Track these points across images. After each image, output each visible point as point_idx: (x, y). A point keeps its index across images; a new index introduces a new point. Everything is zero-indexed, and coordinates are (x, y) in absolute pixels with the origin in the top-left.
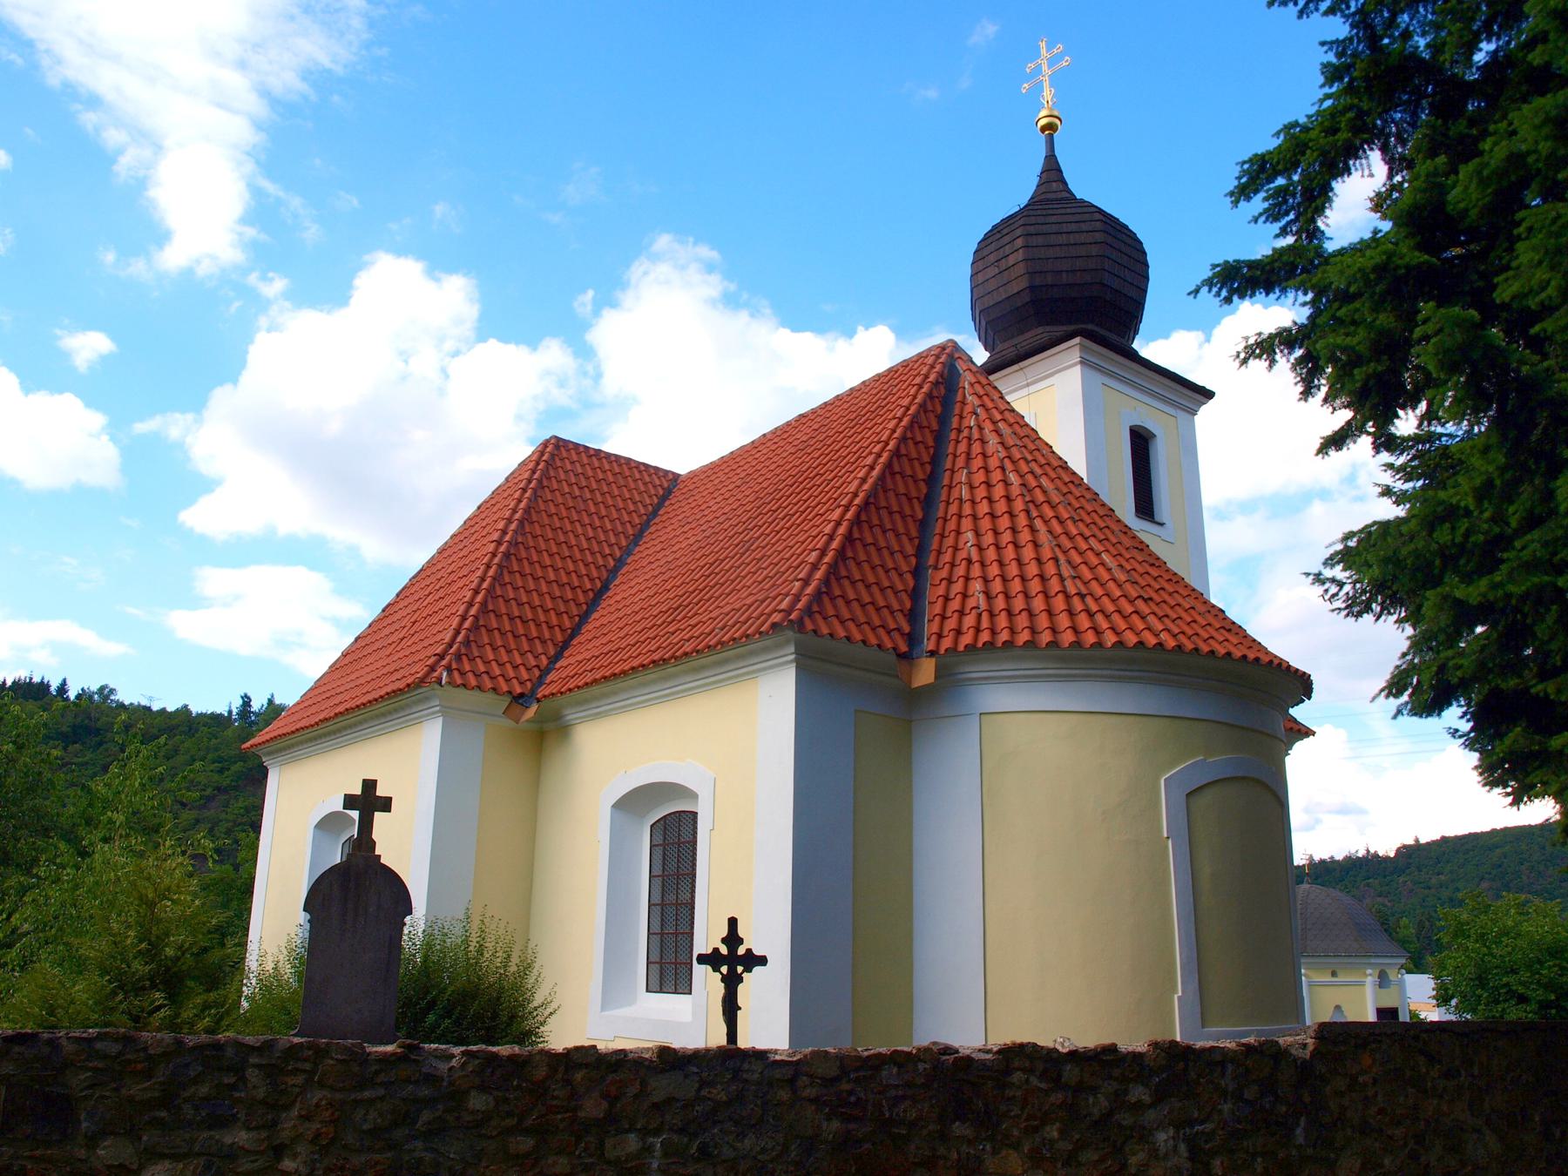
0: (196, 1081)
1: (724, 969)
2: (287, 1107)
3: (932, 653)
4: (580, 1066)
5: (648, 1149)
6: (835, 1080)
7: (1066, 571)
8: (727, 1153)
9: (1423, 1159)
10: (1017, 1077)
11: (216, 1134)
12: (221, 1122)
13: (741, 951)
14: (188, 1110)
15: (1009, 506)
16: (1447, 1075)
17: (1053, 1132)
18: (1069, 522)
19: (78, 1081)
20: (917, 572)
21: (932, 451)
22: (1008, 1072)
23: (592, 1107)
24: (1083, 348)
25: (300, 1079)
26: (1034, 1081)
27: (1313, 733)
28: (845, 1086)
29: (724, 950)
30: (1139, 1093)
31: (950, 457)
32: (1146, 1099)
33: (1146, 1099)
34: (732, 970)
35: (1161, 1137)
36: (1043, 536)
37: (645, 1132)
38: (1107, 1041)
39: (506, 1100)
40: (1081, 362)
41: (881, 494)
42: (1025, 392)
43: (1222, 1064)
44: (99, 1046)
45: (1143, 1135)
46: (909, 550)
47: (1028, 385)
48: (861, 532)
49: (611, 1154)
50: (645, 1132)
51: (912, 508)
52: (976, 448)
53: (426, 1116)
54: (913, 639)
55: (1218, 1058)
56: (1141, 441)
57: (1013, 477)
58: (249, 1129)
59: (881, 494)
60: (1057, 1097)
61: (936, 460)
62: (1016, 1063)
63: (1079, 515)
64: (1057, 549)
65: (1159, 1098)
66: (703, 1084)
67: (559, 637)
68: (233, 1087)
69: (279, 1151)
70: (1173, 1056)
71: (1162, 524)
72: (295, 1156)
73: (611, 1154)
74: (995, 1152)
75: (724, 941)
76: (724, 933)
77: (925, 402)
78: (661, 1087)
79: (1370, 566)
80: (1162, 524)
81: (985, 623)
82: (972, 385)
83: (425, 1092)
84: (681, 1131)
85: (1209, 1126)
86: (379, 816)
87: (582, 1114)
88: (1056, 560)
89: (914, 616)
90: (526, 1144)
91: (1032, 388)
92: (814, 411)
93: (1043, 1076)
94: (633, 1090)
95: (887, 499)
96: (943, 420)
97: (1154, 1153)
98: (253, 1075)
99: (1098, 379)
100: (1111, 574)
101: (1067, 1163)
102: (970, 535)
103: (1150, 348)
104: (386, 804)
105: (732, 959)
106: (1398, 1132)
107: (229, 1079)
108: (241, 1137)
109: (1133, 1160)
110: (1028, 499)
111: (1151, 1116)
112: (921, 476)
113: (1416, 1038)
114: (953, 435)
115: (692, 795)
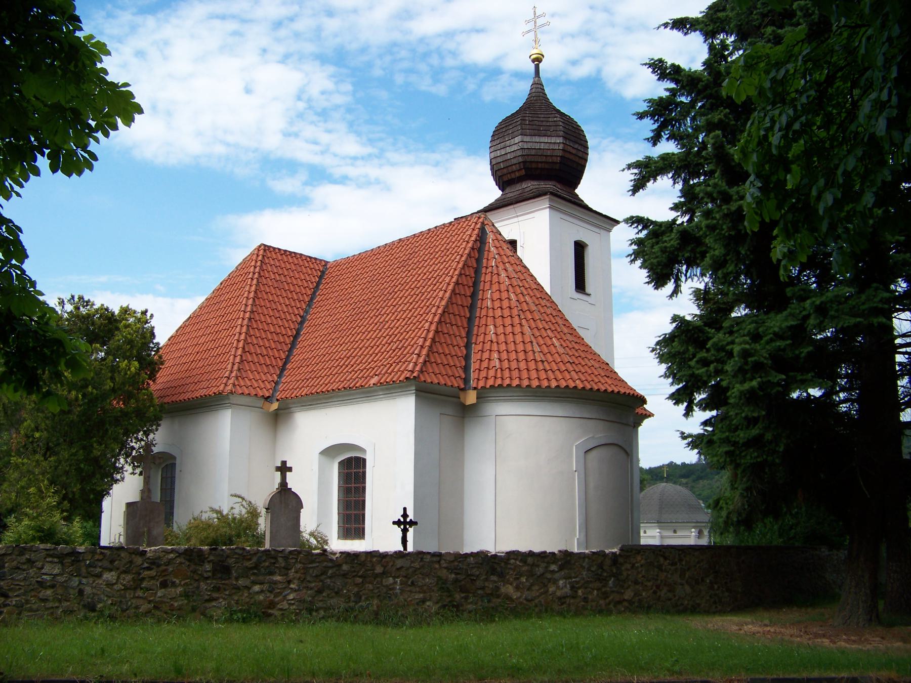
0: (264, 561)
1: (402, 527)
2: (290, 569)
3: (475, 388)
4: (375, 556)
5: (395, 583)
6: (453, 561)
7: (537, 349)
8: (420, 584)
9: (658, 594)
10: (512, 561)
11: (271, 577)
12: (272, 573)
13: (408, 520)
14: (263, 570)
15: (520, 374)
16: (673, 564)
17: (524, 580)
18: (538, 321)
19: (231, 561)
20: (468, 346)
21: (473, 279)
22: (508, 559)
23: (379, 569)
24: (550, 200)
25: (294, 561)
26: (518, 563)
27: (653, 415)
28: (456, 564)
29: (402, 520)
30: (553, 567)
31: (482, 283)
32: (556, 569)
33: (556, 569)
34: (405, 527)
35: (561, 582)
36: (526, 329)
37: (394, 577)
38: (543, 550)
39: (353, 567)
40: (549, 207)
41: (450, 306)
42: (516, 220)
43: (584, 558)
44: (236, 551)
45: (555, 582)
46: (464, 335)
47: (517, 216)
48: (442, 328)
49: (384, 584)
50: (394, 577)
51: (465, 312)
52: (495, 278)
53: (330, 572)
54: (466, 380)
55: (582, 556)
56: (580, 248)
57: (512, 296)
58: (280, 576)
59: (450, 306)
60: (525, 568)
61: (475, 284)
62: (512, 557)
63: (543, 317)
64: (532, 336)
65: (561, 568)
66: (412, 562)
67: (280, 364)
68: (274, 563)
69: (289, 582)
70: (566, 554)
71: (589, 295)
72: (294, 583)
73: (384, 584)
74: (504, 585)
75: (402, 516)
76: (402, 513)
77: (470, 252)
78: (399, 563)
79: (468, 596)
80: (589, 295)
81: (499, 375)
82: (493, 240)
83: (330, 564)
84: (405, 577)
85: (577, 579)
86: (288, 473)
87: (376, 572)
88: (532, 342)
89: (466, 369)
90: (359, 580)
91: (520, 218)
92: (408, 239)
93: (521, 561)
94: (391, 564)
95: (453, 308)
96: (479, 261)
97: (558, 587)
98: (280, 560)
99: (559, 215)
100: (556, 350)
101: (528, 590)
102: (492, 327)
103: (584, 191)
104: (290, 469)
105: (405, 523)
106: (649, 584)
107: (273, 561)
108: (278, 578)
109: (551, 590)
110: (519, 309)
111: (557, 576)
112: (469, 294)
113: (660, 551)
114: (484, 270)
115: (363, 451)
